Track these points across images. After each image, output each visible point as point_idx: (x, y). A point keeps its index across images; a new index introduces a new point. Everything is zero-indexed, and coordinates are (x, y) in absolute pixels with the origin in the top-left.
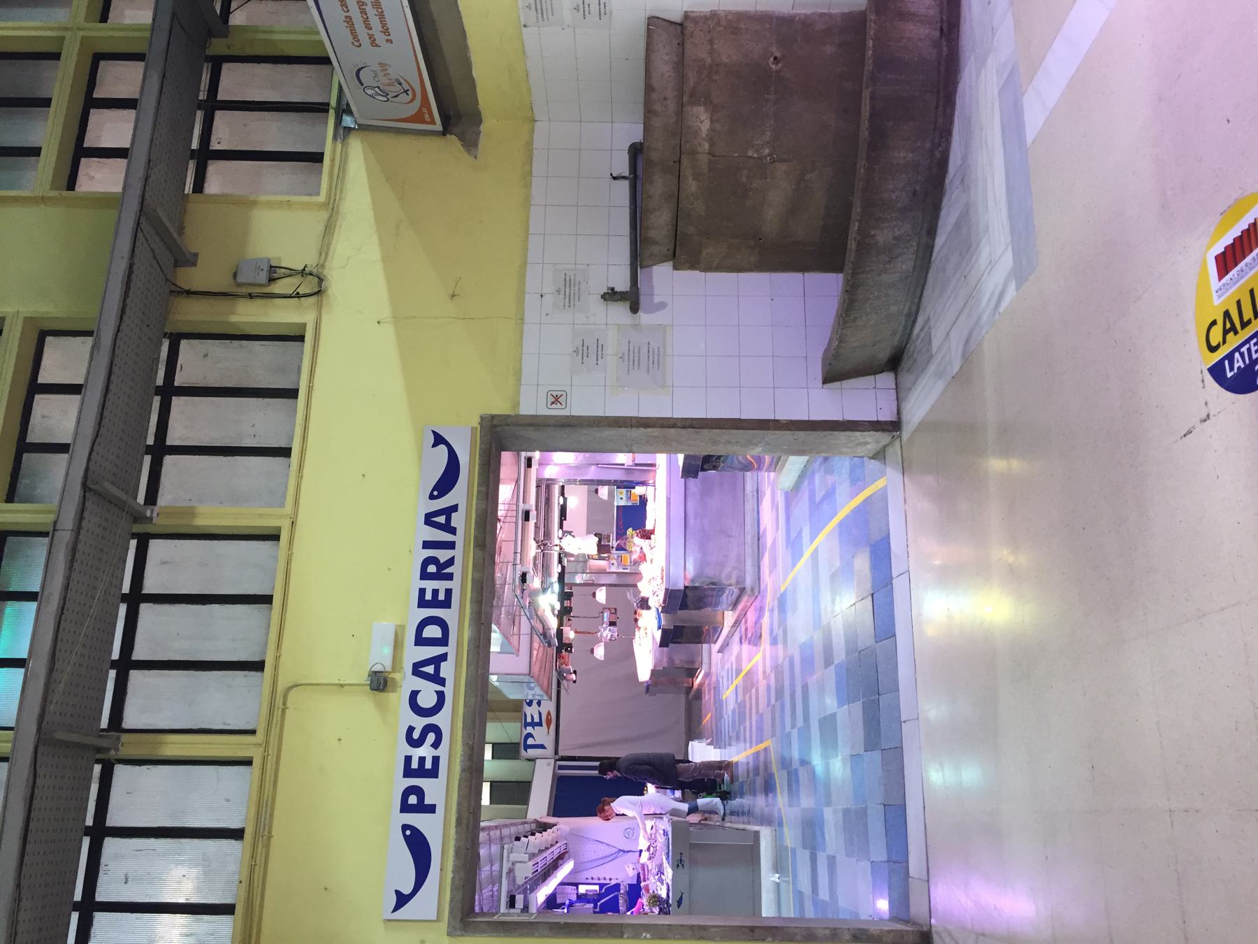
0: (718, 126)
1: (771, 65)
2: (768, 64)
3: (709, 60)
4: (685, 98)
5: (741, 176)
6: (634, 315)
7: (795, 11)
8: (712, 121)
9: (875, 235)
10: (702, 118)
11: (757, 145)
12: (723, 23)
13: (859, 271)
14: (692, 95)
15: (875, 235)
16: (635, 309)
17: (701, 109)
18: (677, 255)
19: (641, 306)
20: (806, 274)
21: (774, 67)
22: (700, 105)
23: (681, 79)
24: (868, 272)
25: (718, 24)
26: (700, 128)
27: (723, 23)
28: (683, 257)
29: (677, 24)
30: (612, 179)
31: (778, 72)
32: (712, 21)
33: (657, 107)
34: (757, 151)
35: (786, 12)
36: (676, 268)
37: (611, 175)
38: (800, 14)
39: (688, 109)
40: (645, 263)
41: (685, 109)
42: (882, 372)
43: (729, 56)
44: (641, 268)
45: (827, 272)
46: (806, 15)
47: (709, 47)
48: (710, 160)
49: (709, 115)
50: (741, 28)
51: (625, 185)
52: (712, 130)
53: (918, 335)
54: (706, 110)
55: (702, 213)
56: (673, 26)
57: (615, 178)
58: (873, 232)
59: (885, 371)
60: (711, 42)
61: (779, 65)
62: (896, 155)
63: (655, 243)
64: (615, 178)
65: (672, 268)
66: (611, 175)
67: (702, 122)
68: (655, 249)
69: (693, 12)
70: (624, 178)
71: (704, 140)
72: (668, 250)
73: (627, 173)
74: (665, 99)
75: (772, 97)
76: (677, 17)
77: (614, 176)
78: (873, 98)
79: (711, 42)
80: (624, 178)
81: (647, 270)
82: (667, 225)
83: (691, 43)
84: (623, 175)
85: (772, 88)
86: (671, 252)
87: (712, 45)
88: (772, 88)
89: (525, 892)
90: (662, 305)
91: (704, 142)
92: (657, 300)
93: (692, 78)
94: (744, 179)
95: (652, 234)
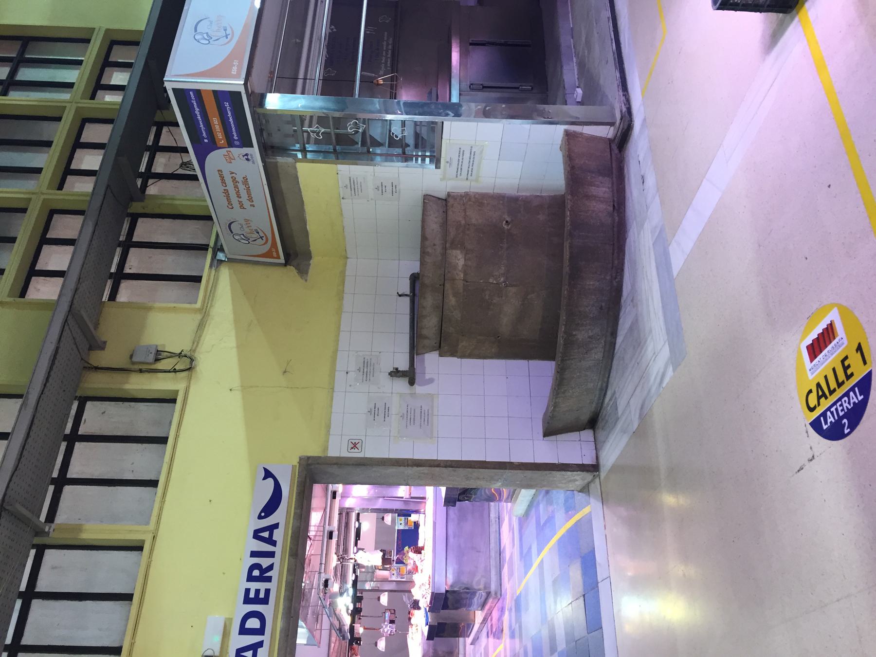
0: (469, 263)
3: (463, 222)
4: (448, 245)
9: (575, 335)
11: (496, 275)
12: (473, 200)
14: (452, 243)
15: (575, 335)
16: (412, 383)
17: (458, 252)
24: (572, 359)
25: (470, 200)
26: (457, 264)
31: (508, 230)
33: (429, 250)
36: (441, 355)
37: (398, 293)
38: (522, 196)
41: (448, 251)
42: (584, 429)
44: (417, 355)
46: (527, 197)
51: (407, 300)
52: (465, 265)
53: (608, 404)
54: (461, 252)
56: (440, 201)
58: (574, 333)
61: (510, 226)
64: (400, 296)
66: (398, 293)
67: (459, 260)
68: (426, 342)
70: (406, 295)
72: (435, 343)
73: (408, 293)
76: (443, 195)
79: (465, 210)
80: (406, 295)
81: (420, 357)
82: (435, 326)
84: (405, 293)
86: (438, 345)
87: (465, 212)
88: (505, 240)
90: (431, 381)
92: (427, 377)
93: (452, 232)
94: (487, 297)
95: (425, 332)
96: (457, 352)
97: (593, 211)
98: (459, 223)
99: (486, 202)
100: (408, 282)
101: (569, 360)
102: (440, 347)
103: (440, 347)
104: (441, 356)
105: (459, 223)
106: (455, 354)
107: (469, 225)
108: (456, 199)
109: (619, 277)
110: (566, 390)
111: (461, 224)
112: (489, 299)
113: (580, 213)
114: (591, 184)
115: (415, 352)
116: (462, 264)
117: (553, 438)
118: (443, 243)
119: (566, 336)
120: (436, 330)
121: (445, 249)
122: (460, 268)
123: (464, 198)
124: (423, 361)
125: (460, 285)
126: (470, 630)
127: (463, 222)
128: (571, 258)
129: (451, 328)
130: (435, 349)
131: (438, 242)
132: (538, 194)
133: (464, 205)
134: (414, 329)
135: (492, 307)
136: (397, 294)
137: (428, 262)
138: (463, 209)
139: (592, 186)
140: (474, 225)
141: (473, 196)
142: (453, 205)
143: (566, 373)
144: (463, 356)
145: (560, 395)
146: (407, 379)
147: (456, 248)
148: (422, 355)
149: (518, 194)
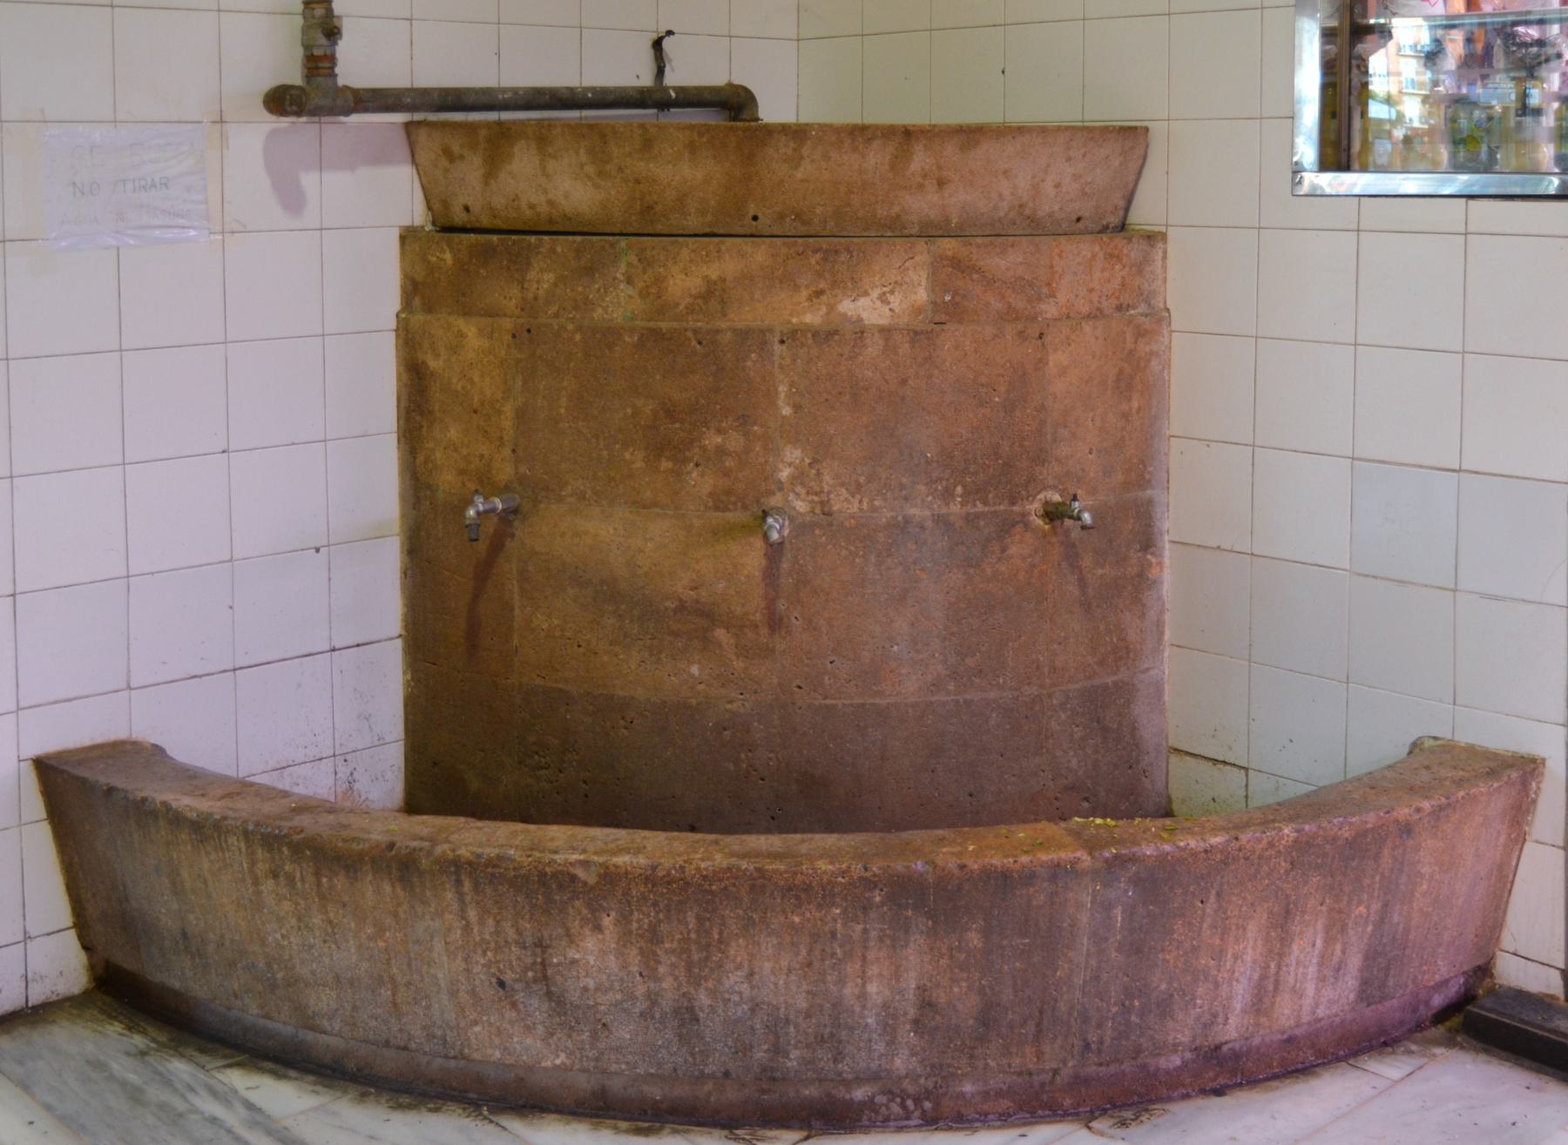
0: (873, 348)
1: (1041, 496)
2: (1044, 488)
3: (1050, 309)
4: (949, 246)
5: (719, 431)
6: (259, 101)
7: (1168, 551)
8: (886, 331)
9: (598, 928)
10: (895, 301)
11: (819, 474)
12: (1144, 348)
13: (467, 885)
14: (957, 264)
15: (598, 928)
16: (280, 101)
17: (922, 295)
18: (456, 237)
19: (285, 122)
20: (399, 643)
21: (1035, 507)
22: (932, 290)
23: (997, 232)
24: (463, 915)
25: (1140, 334)
26: (866, 294)
27: (1144, 348)
28: (448, 256)
29: (1127, 210)
30: (655, 36)
31: (1023, 519)
32: (1146, 316)
33: (920, 159)
34: (799, 477)
35: (1166, 525)
36: (408, 236)
37: (670, 33)
38: (1160, 564)
39: (923, 254)
40: (422, 136)
41: (921, 244)
42: (86, 948)
43: (1063, 372)
44: (408, 126)
45: (406, 706)
46: (1155, 583)
47: (1085, 309)
48: (771, 330)
49: (904, 321)
50: (1129, 399)
51: (634, 73)
52: (861, 332)
53: (225, 1097)
54: (917, 311)
55: (598, 313)
56: (1122, 203)
57: (657, 45)
58: (607, 921)
59: (90, 958)
60: (1096, 315)
61: (1039, 522)
62: (873, 970)
63: (490, 174)
64: (657, 45)
65: (408, 223)
66: (670, 33)
67: (883, 299)
68: (471, 169)
69: (1164, 258)
70: (660, 72)
71: (831, 308)
72: (467, 209)
73: (673, 79)
74: (941, 183)
75: (956, 508)
76: (1144, 213)
77: (666, 43)
78: (1057, 872)
79: (1096, 315)
80: (660, 72)
81: (399, 141)
82: (551, 203)
83: (1094, 256)
84: (667, 70)
85: (980, 508)
86: (459, 218)
87: (1089, 316)
88: (980, 508)
89: (661, 312)
90: (292, 200)
91: (824, 309)
92: (309, 181)
93: (1006, 262)
94: (713, 440)
95: (522, 163)
96: (429, 309)
97: (1219, 955)
98: (1045, 290)
99: (1135, 404)
100: (719, 80)
101: (461, 896)
102: (448, 229)
103: (448, 229)
104: (403, 239)
105: (1045, 290)
106: (417, 301)
107: (1041, 336)
108: (1140, 272)
109: (896, 1109)
110: (291, 880)
111: (1040, 299)
112: (704, 448)
113: (1212, 898)
114: (1336, 927)
115: (418, 117)
116: (864, 315)
117: (35, 805)
118: (948, 221)
119: (592, 880)
120: (532, 206)
121: (931, 231)
122: (847, 306)
123: (1142, 308)
124: (379, 158)
125: (747, 314)
126: (506, 116)
127: (1050, 309)
128: (1003, 881)
129: (549, 277)
130: (437, 206)
131: (959, 200)
132: (1167, 636)
133: (1119, 308)
134: (528, 106)
135: (665, 464)
136: (662, 30)
137: (863, 156)
138: (1105, 304)
139: (1328, 929)
140: (1041, 363)
141: (1155, 347)
142: (1119, 259)
143: (387, 888)
144: (409, 341)
145: (260, 854)
146: (295, 77)
147: (936, 285)
148: (404, 151)
149: (1167, 546)
